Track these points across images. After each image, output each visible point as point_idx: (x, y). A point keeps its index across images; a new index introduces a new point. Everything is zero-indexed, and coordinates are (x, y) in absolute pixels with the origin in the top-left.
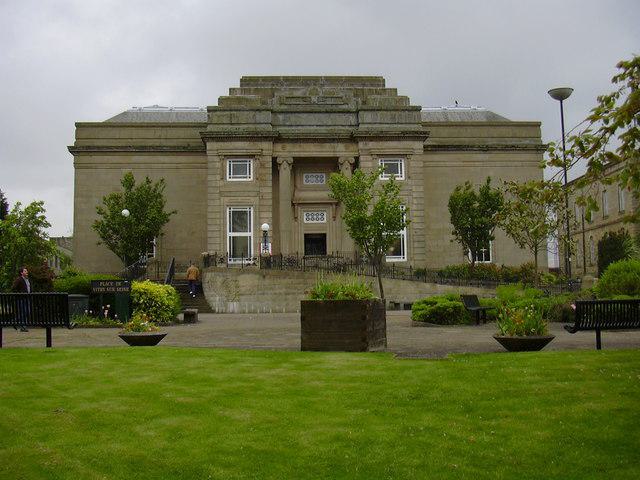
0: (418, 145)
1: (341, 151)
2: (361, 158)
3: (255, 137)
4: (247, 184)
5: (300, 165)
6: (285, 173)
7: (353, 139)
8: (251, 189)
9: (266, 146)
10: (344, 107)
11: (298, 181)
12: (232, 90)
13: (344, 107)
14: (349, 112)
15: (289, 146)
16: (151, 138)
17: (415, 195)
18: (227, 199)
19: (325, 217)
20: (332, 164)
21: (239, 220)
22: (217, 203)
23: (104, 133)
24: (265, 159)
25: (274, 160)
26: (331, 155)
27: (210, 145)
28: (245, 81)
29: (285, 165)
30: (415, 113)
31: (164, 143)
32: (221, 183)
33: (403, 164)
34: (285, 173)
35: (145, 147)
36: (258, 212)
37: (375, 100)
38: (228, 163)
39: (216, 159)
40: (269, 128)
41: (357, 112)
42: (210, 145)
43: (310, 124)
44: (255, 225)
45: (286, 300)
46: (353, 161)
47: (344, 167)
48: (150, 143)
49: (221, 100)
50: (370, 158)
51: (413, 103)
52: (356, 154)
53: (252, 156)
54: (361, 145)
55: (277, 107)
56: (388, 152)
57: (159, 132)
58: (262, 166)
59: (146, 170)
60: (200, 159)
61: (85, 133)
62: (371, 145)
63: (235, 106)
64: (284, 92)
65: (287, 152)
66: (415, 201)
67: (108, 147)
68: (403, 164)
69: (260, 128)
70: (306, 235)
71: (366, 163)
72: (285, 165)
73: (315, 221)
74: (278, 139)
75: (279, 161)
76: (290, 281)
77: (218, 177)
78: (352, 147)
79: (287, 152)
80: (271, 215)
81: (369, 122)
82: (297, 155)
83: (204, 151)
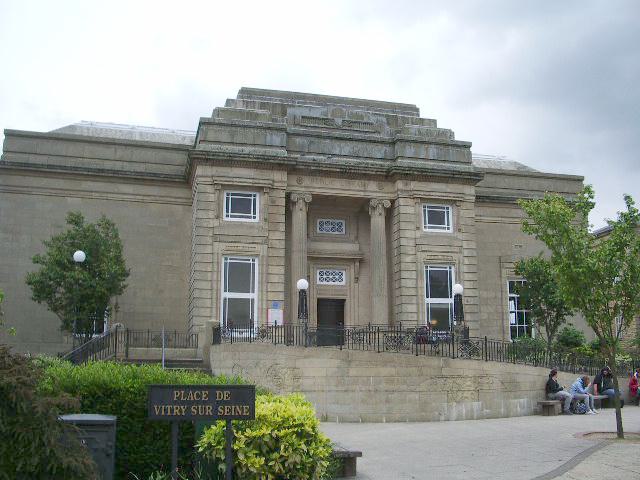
0: (470, 191)
1: (372, 190)
2: (402, 201)
3: (263, 163)
4: (251, 226)
5: (321, 206)
6: (300, 216)
7: (389, 176)
8: (255, 232)
9: (279, 177)
10: (375, 135)
11: (311, 229)
12: (229, 102)
13: (375, 135)
14: (383, 142)
15: (307, 181)
16: (110, 160)
17: (466, 253)
18: (223, 246)
19: (344, 277)
20: (360, 210)
21: (239, 276)
22: (209, 249)
23: (48, 147)
24: (275, 193)
25: (288, 196)
26: (361, 194)
27: (200, 170)
28: (245, 93)
29: (301, 205)
30: (466, 150)
31: (127, 167)
32: (216, 223)
33: (259, 200)
34: (300, 216)
35: (102, 171)
36: (267, 262)
37: (413, 130)
38: (225, 196)
39: (210, 189)
40: (283, 153)
41: (393, 143)
42: (200, 170)
43: (343, 153)
44: (261, 283)
45: (387, 401)
46: (388, 204)
47: (377, 213)
48: (108, 165)
49: (217, 112)
50: (411, 202)
51: (458, 137)
52: (392, 196)
53: (453, 202)
54: (400, 185)
55: (292, 129)
56: (435, 195)
57: (121, 153)
58: (273, 203)
59: (93, 205)
60: (179, 192)
61: (19, 144)
62: (414, 185)
63: (236, 120)
64: (299, 112)
65: (311, 187)
66: (466, 262)
67: (49, 166)
68: (259, 200)
69: (271, 151)
70: (318, 300)
71: (407, 209)
72: (301, 205)
73: (331, 283)
74: (292, 169)
75: (294, 197)
76: (393, 371)
77: (211, 214)
78: (388, 187)
79: (311, 187)
80: (282, 271)
81: (409, 156)
82: (317, 191)
83: (186, 180)
